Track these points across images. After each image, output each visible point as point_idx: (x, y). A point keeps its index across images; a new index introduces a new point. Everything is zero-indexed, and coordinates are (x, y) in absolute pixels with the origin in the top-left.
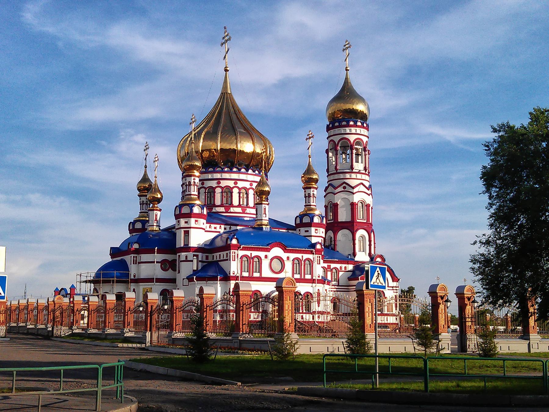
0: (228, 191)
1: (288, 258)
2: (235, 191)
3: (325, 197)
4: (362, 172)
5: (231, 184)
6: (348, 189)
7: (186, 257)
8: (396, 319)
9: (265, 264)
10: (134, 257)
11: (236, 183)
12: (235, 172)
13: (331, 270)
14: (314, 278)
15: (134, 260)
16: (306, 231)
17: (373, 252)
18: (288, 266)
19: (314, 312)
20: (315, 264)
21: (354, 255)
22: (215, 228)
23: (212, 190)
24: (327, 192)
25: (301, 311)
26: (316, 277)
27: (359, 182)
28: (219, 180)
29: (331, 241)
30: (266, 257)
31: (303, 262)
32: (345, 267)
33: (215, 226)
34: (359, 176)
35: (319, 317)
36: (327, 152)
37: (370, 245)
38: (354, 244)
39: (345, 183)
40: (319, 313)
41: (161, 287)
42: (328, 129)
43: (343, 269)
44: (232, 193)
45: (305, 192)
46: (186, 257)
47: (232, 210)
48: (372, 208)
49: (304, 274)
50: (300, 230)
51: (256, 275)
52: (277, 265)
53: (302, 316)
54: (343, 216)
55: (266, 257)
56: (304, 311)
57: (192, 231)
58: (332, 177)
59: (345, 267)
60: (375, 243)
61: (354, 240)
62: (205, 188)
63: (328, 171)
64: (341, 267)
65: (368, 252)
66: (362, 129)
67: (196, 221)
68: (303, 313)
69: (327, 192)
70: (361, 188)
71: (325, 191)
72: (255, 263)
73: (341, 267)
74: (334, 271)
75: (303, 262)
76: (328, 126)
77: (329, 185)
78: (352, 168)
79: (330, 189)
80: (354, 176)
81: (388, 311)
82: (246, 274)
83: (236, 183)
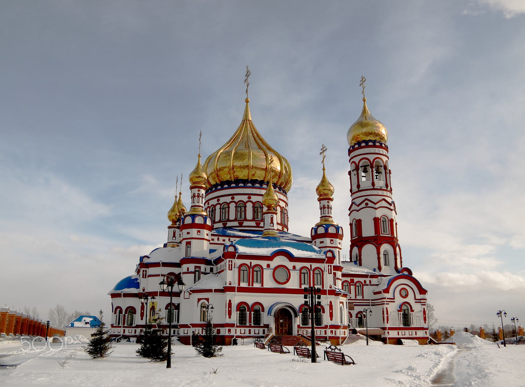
0: (241, 207)
1: (294, 267)
2: (249, 206)
3: (349, 215)
4: (383, 188)
5: (245, 198)
6: (370, 204)
7: (188, 268)
8: (426, 333)
9: (267, 274)
10: (143, 271)
11: (249, 198)
13: (355, 285)
14: (325, 289)
15: (143, 274)
17: (399, 266)
18: (295, 276)
19: (326, 327)
20: (326, 274)
21: (380, 268)
22: (224, 240)
23: (225, 207)
24: (351, 210)
25: (248, 324)
26: (327, 288)
27: (364, 198)
28: (233, 195)
29: (357, 257)
30: (268, 266)
31: (311, 272)
33: (224, 238)
34: (380, 192)
35: (332, 332)
37: (396, 259)
38: (379, 258)
39: (366, 199)
41: (167, 300)
42: (350, 152)
43: (368, 283)
44: (245, 207)
45: (320, 203)
46: (188, 268)
47: (245, 223)
48: (396, 224)
49: (314, 285)
50: (315, 242)
51: (257, 285)
52: (281, 275)
54: (368, 231)
55: (268, 266)
56: (253, 325)
57: (193, 242)
58: (355, 196)
60: (401, 258)
61: (378, 254)
62: (221, 205)
63: (351, 191)
64: (365, 281)
66: (381, 149)
67: (199, 231)
68: (250, 326)
69: (351, 210)
70: (384, 204)
71: (349, 209)
73: (365, 281)
74: (358, 284)
75: (311, 272)
76: (349, 150)
77: (353, 203)
78: (373, 184)
79: (354, 207)
80: (374, 192)
82: (244, 285)
83: (249, 198)
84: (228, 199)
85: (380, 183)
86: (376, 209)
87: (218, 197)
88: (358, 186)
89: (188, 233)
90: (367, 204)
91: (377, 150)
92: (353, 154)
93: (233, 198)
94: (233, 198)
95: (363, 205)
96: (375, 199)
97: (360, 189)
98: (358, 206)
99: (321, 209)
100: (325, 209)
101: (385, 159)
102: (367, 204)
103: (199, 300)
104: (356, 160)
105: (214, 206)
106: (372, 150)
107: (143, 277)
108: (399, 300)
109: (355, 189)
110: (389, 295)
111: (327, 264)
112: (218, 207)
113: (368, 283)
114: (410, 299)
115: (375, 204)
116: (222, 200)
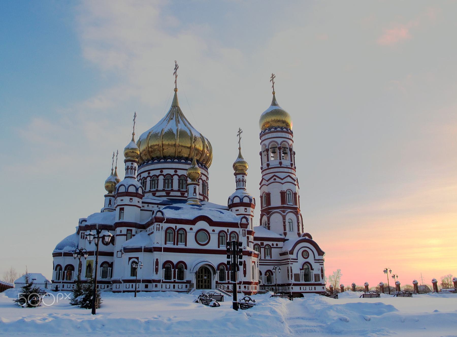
2: (176, 178)
3: (260, 189)
5: (172, 172)
6: (278, 180)
7: (121, 231)
9: (191, 237)
10: (82, 233)
11: (176, 172)
12: (176, 163)
15: (82, 236)
16: (237, 210)
18: (214, 238)
23: (155, 179)
24: (262, 184)
27: (273, 174)
28: (161, 170)
31: (228, 236)
32: (277, 245)
34: (286, 170)
35: (245, 287)
36: (261, 154)
39: (275, 176)
40: (245, 283)
43: (275, 246)
44: (172, 180)
45: (236, 177)
53: (228, 286)
58: (264, 173)
59: (277, 245)
62: (151, 177)
63: (262, 168)
64: (273, 245)
65: (296, 232)
66: (287, 134)
69: (262, 184)
71: (260, 184)
72: (180, 235)
73: (273, 245)
75: (228, 236)
77: (263, 179)
78: (281, 163)
80: (281, 170)
81: (315, 281)
83: (176, 172)
84: (158, 173)
85: (286, 162)
86: (283, 184)
87: (149, 171)
88: (268, 165)
89: (122, 200)
90: (275, 179)
91: (284, 135)
92: (263, 138)
93: (161, 172)
94: (161, 172)
95: (272, 180)
96: (282, 175)
97: (270, 167)
98: (268, 181)
99: (237, 182)
100: (241, 183)
101: (290, 142)
102: (275, 179)
103: (130, 258)
104: (267, 142)
105: (145, 178)
106: (279, 134)
107: (81, 238)
108: (301, 260)
109: (265, 166)
110: (294, 256)
111: (242, 229)
112: (149, 179)
113: (275, 246)
114: (311, 259)
115: (282, 179)
116: (152, 173)
